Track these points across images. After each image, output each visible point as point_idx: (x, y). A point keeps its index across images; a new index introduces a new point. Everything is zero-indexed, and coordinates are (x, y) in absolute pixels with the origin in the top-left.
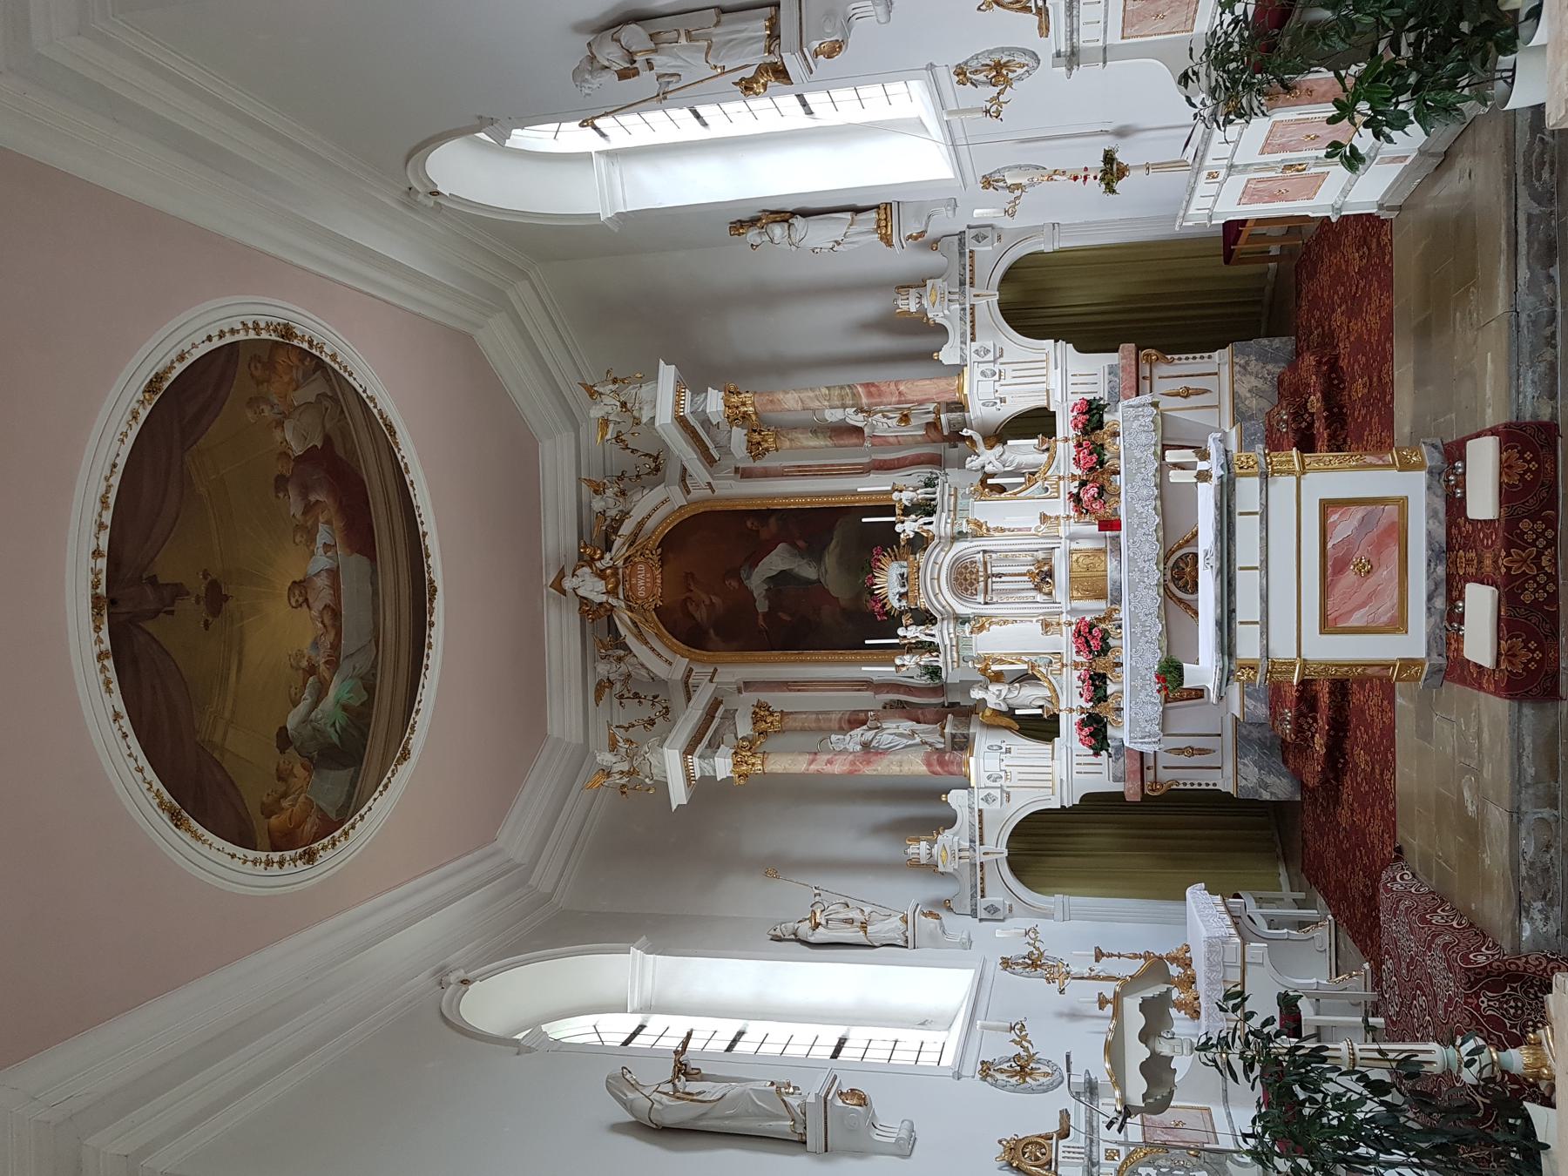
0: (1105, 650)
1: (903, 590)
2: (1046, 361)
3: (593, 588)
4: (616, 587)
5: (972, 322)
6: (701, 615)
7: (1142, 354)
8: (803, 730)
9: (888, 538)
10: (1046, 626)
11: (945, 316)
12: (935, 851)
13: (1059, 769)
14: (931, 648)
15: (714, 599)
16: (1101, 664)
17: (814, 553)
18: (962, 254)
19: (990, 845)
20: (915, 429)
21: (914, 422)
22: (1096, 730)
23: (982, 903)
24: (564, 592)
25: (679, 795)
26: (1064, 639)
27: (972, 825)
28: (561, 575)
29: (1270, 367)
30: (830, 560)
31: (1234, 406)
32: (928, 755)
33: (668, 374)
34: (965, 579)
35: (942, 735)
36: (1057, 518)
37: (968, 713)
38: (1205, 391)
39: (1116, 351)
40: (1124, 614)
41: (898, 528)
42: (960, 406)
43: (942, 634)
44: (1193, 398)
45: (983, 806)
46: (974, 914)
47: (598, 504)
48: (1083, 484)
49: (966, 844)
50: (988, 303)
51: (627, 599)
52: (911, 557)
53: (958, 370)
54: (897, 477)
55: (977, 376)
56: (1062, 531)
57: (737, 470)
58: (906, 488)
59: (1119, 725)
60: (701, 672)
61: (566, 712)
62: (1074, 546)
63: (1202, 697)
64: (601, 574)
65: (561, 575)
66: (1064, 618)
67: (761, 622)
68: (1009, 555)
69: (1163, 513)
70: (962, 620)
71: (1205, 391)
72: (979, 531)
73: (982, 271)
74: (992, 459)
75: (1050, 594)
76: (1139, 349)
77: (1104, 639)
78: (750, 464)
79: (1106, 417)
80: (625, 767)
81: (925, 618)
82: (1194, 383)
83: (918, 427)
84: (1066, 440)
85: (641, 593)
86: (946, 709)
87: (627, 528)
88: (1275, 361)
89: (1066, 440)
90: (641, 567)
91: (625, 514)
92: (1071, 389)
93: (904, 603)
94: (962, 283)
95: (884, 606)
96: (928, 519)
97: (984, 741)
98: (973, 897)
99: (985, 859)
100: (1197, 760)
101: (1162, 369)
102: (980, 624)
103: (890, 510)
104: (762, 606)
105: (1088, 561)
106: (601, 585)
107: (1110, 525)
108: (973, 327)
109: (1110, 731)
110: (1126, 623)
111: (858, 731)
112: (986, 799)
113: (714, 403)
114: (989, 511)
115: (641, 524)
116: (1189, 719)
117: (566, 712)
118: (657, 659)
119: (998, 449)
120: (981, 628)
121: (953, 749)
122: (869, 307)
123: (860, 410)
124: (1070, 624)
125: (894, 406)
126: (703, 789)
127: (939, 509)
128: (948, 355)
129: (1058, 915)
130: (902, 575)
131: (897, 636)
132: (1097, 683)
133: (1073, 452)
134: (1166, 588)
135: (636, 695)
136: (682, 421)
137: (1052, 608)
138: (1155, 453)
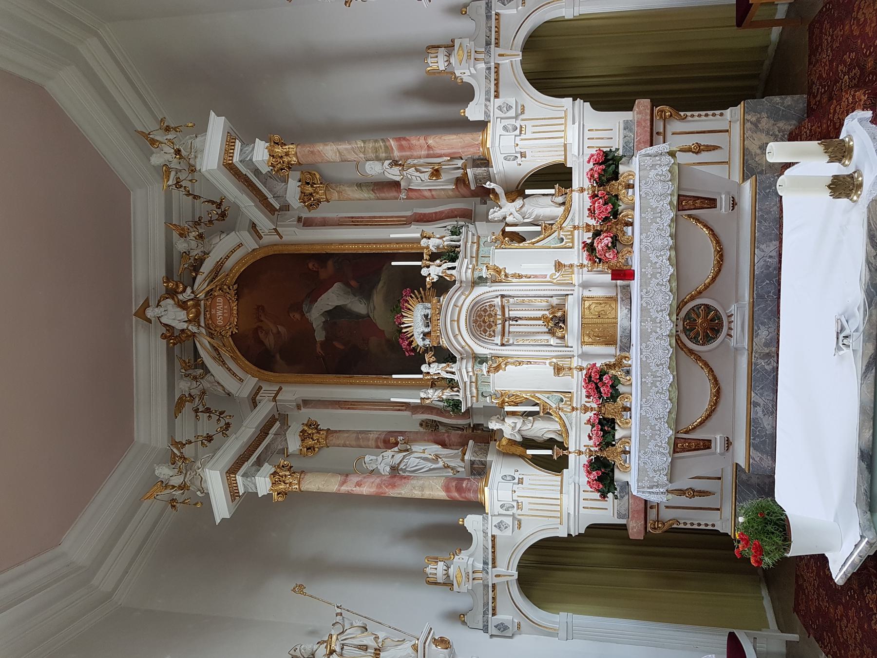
0: (615, 396)
1: (427, 330)
2: (565, 117)
3: (175, 317)
4: (198, 315)
5: (497, 80)
6: (269, 341)
7: (656, 110)
8: (345, 446)
9: (413, 282)
10: (558, 370)
11: (472, 75)
12: (451, 571)
13: (568, 503)
14: (452, 384)
15: (281, 328)
16: (610, 411)
17: (365, 291)
18: (489, 17)
19: (501, 569)
20: (445, 184)
21: (444, 177)
22: (603, 472)
23: (493, 621)
24: (149, 321)
25: (221, 509)
26: (574, 381)
27: (485, 548)
28: (146, 305)
29: (781, 124)
30: (378, 298)
31: (745, 163)
32: (449, 479)
33: (217, 126)
34: (483, 321)
35: (463, 460)
36: (571, 266)
37: (486, 438)
38: (715, 148)
39: (630, 108)
40: (634, 359)
41: (424, 272)
42: (484, 162)
43: (462, 371)
44: (704, 154)
45: (496, 532)
46: (485, 629)
47: (181, 245)
48: (597, 234)
49: (480, 566)
50: (511, 62)
51: (207, 327)
52: (435, 300)
53: (482, 126)
54: (428, 228)
55: (499, 130)
56: (576, 279)
57: (299, 219)
58: (437, 238)
59: (626, 470)
60: (268, 389)
61: (151, 424)
62: (587, 293)
63: (709, 448)
64: (183, 305)
65: (146, 305)
66: (575, 362)
67: (319, 349)
68: (524, 301)
69: (677, 263)
70: (480, 360)
71: (715, 148)
72: (499, 276)
73: (507, 32)
74: (513, 210)
75: (563, 338)
76: (654, 104)
77: (613, 387)
78: (306, 214)
79: (622, 169)
80: (177, 481)
81: (446, 356)
82: (705, 140)
83: (448, 182)
84: (582, 190)
85: (220, 322)
86: (467, 432)
87: (207, 267)
88: (786, 118)
89: (582, 190)
90: (220, 300)
91: (206, 254)
92: (588, 143)
93: (427, 342)
94: (488, 44)
95: (411, 343)
96: (451, 265)
97: (500, 469)
98: (485, 613)
99: (496, 580)
100: (697, 501)
101: (676, 126)
102: (497, 364)
103: (419, 257)
104: (320, 336)
105: (599, 308)
106: (182, 315)
107: (623, 274)
108: (497, 85)
109: (618, 475)
110: (635, 371)
111: (389, 453)
112: (499, 526)
113: (260, 152)
114: (508, 259)
115: (219, 266)
116: (697, 465)
117: (151, 424)
118: (232, 378)
119: (519, 202)
120: (497, 369)
121: (472, 474)
122: (407, 75)
123: (395, 163)
124: (581, 369)
125: (426, 164)
126: (247, 505)
127: (461, 255)
128: (473, 112)
129: (562, 634)
130: (426, 316)
131: (421, 372)
132: (605, 426)
133: (588, 203)
134: (678, 339)
135: (208, 410)
136: (231, 168)
137: (564, 351)
138: (671, 203)
